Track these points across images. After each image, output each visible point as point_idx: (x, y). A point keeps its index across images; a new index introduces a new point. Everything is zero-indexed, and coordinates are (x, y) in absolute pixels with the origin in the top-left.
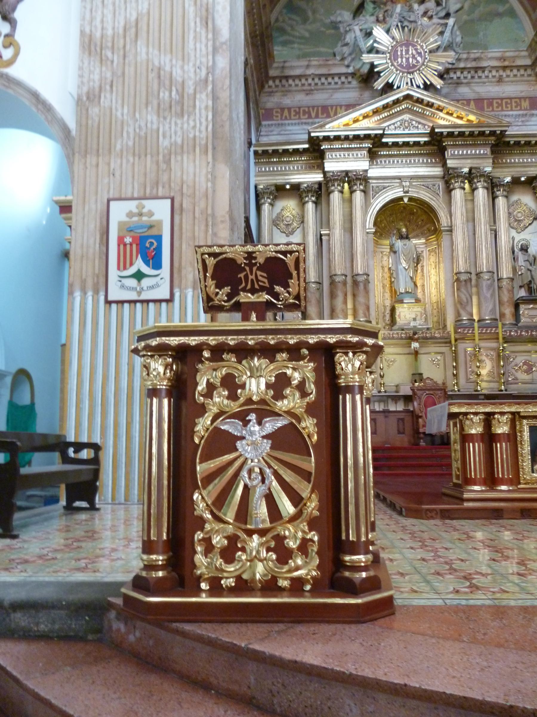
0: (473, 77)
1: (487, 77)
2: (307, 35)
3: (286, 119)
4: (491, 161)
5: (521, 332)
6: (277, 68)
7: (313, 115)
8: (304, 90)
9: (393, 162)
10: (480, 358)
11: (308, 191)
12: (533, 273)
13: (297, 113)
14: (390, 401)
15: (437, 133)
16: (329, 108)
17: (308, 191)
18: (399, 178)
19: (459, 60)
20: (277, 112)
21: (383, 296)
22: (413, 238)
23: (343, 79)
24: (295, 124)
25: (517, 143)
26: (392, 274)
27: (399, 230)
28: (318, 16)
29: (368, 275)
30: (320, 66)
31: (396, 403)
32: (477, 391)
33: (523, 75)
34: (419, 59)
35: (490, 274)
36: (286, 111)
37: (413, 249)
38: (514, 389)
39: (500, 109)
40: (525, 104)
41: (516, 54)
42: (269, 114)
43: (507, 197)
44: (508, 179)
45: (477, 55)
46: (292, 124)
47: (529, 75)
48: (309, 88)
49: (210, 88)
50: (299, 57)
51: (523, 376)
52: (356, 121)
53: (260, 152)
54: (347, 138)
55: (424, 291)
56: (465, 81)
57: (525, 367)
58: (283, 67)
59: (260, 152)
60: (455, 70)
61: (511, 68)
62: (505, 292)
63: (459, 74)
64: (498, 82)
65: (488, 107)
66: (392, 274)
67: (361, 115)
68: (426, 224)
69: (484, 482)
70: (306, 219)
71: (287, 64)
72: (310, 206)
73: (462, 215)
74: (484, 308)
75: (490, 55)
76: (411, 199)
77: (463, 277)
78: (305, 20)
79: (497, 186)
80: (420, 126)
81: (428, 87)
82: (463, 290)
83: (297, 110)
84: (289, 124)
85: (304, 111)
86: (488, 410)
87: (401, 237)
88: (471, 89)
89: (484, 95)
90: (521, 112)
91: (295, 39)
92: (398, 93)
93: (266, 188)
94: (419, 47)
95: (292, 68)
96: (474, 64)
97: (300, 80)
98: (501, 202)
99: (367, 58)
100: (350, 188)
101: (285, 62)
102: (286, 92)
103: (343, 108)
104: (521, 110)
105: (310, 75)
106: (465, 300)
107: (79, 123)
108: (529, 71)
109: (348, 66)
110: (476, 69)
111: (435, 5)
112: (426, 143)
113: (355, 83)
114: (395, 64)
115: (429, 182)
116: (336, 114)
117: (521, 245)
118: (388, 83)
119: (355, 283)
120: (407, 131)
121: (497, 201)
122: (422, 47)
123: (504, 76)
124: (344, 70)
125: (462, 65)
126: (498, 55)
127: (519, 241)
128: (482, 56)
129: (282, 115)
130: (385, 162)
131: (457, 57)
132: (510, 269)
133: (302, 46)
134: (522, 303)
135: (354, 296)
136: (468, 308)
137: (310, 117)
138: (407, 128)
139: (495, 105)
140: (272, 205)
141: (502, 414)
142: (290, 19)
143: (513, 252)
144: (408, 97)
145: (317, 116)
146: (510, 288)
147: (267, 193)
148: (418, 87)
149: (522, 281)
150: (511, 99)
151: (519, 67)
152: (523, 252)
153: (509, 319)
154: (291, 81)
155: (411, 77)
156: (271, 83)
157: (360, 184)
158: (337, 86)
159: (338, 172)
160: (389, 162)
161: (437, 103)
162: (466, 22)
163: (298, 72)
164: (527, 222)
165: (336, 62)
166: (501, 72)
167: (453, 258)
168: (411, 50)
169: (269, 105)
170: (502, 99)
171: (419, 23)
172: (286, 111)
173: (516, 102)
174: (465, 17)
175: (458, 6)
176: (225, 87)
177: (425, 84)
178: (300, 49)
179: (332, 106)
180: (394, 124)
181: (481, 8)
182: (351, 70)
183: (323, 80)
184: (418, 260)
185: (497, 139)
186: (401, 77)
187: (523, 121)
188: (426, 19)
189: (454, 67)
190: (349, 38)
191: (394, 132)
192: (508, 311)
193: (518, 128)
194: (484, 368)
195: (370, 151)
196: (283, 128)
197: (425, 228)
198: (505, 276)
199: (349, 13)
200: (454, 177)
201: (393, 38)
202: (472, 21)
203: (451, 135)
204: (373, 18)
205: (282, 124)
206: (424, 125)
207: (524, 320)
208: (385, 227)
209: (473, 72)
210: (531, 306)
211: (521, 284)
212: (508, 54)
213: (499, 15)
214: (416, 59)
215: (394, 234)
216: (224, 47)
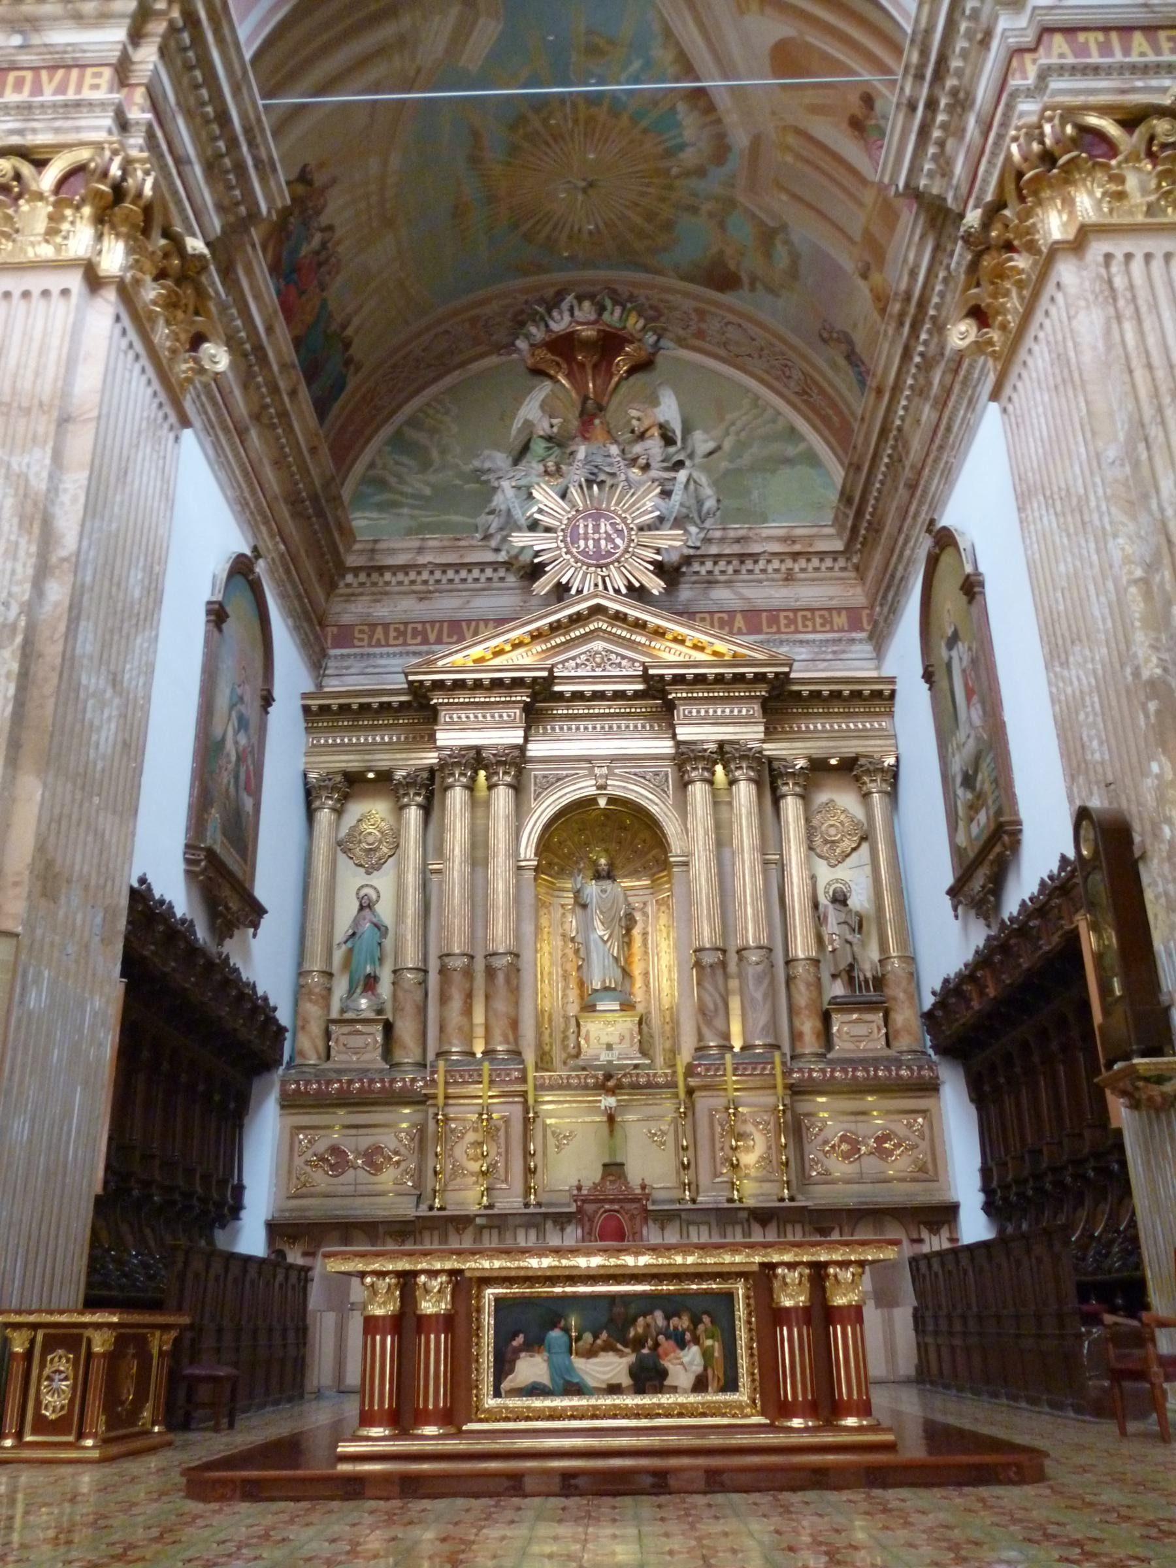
0: (736, 572)
1: (763, 571)
2: (428, 491)
3: (379, 645)
4: (762, 728)
6: (362, 551)
7: (432, 637)
8: (414, 592)
9: (578, 728)
10: (741, 1128)
11: (408, 785)
12: (855, 948)
13: (401, 634)
14: (549, 1225)
15: (653, 676)
16: (464, 624)
17: (408, 785)
18: (588, 759)
19: (707, 541)
20: (361, 632)
21: (564, 996)
22: (625, 876)
23: (489, 572)
24: (395, 655)
25: (815, 695)
26: (580, 950)
27: (595, 863)
28: (449, 457)
29: (517, 956)
30: (443, 549)
31: (562, 1230)
32: (731, 1200)
33: (817, 569)
34: (618, 541)
35: (763, 952)
36: (379, 629)
37: (621, 898)
38: (820, 1196)
39: (792, 628)
40: (841, 620)
41: (814, 531)
42: (345, 637)
43: (802, 797)
44: (801, 763)
45: (741, 533)
46: (388, 655)
47: (843, 569)
48: (424, 588)
49: (19, 639)
50: (409, 532)
51: (839, 1168)
52: (498, 653)
53: (314, 709)
54: (478, 685)
55: (647, 985)
56: (722, 578)
57: (844, 1147)
58: (373, 551)
59: (314, 709)
60: (702, 558)
61: (808, 556)
62: (802, 987)
63: (709, 565)
64: (786, 579)
65: (770, 626)
66: (580, 950)
67: (506, 641)
68: (651, 849)
69: (812, 1409)
70: (402, 842)
71: (381, 546)
72: (413, 815)
73: (706, 833)
74: (750, 1021)
75: (765, 533)
76: (612, 800)
77: (709, 959)
78: (426, 465)
79: (781, 775)
80: (624, 662)
81: (638, 593)
82: (707, 985)
83: (402, 628)
84: (381, 655)
85: (414, 629)
86: (403, 1265)
87: (598, 876)
88: (736, 593)
89: (761, 604)
90: (829, 636)
91: (404, 500)
92: (578, 603)
93: (329, 776)
94: (618, 520)
95: (392, 552)
96: (737, 549)
97: (407, 574)
98: (791, 807)
99: (520, 539)
100: (488, 778)
101: (376, 541)
102: (380, 595)
103: (491, 624)
104: (832, 631)
105: (424, 566)
106: (711, 1006)
108: (841, 562)
109: (497, 550)
110: (742, 558)
111: (662, 443)
112: (637, 695)
113: (512, 579)
114: (574, 550)
115: (650, 769)
116: (476, 633)
117: (835, 892)
118: (559, 584)
120: (598, 672)
121: (782, 803)
122: (624, 520)
123: (797, 569)
124: (490, 557)
125: (714, 550)
126: (781, 532)
127: (829, 884)
128: (751, 534)
129: (371, 637)
130: (561, 729)
131: (702, 535)
132: (812, 941)
133: (417, 512)
134: (838, 1011)
136: (719, 1023)
137: (425, 641)
138: (599, 666)
139: (783, 622)
140: (339, 812)
141: (433, 1274)
142: (397, 463)
143: (816, 906)
144: (598, 610)
145: (439, 641)
146: (811, 979)
147: (326, 787)
148: (617, 591)
149: (836, 965)
150: (812, 610)
151: (822, 555)
152: (838, 906)
153: (810, 1044)
154: (388, 576)
155: (605, 572)
156: (349, 578)
157: (505, 773)
158: (478, 586)
159: (462, 748)
160: (570, 729)
161: (653, 621)
162: (727, 473)
163: (401, 559)
164: (847, 844)
165: (474, 543)
166: (789, 563)
167: (690, 920)
168: (605, 526)
169: (346, 619)
170: (795, 611)
171: (623, 477)
172: (379, 629)
173: (822, 616)
174: (724, 465)
175: (711, 445)
176: (56, 636)
177: (630, 587)
178: (412, 517)
179: (469, 622)
180: (573, 658)
181: (754, 450)
182: (502, 557)
183: (438, 575)
184: (629, 922)
185: (773, 688)
186: (585, 574)
187: (834, 652)
188: (635, 470)
189: (699, 552)
190: (498, 501)
191: (573, 674)
192: (808, 1026)
193: (825, 664)
194: (748, 1150)
195: (528, 709)
196: (372, 662)
197: (650, 856)
198: (801, 955)
199: (504, 455)
200: (689, 759)
201: (573, 505)
202: (738, 471)
203: (679, 680)
204: (541, 468)
205: (369, 655)
206: (633, 661)
207: (842, 1047)
208: (572, 854)
209: (735, 562)
210: (855, 1016)
211: (833, 971)
212: (799, 532)
213: (788, 461)
214: (613, 541)
215: (580, 871)
216: (66, 565)
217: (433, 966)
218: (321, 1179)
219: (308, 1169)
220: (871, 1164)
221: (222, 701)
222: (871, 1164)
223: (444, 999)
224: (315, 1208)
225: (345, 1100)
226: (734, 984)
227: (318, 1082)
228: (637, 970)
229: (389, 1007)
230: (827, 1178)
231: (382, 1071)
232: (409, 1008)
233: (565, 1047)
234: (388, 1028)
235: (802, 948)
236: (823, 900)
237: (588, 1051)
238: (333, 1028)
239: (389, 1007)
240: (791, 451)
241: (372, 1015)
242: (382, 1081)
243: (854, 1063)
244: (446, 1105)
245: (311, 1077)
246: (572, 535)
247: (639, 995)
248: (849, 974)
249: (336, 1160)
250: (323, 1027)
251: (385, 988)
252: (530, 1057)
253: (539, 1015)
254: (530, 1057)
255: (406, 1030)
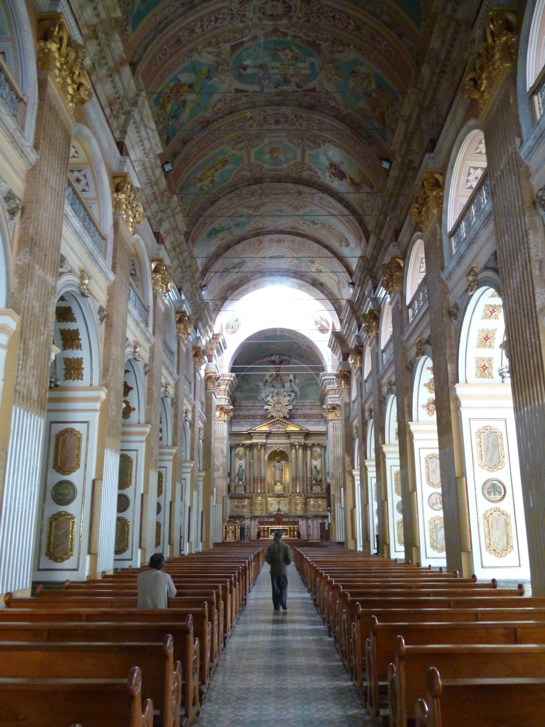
13: (244, 417)
25: (313, 434)
26: (274, 474)
51: (313, 509)
66: (274, 474)
77: (294, 478)
78: (248, 383)
99: (266, 407)
119: (261, 480)
124: (260, 405)
135: (261, 483)
153: (309, 491)
184: (282, 470)
192: (309, 488)
207: (314, 491)
213: (312, 384)
217: (252, 479)
218: (235, 509)
220: (317, 509)
222: (317, 509)
224: (234, 514)
225: (239, 498)
228: (283, 477)
230: (311, 511)
234: (245, 487)
235: (309, 476)
236: (313, 467)
237: (275, 490)
240: (314, 382)
243: (315, 494)
246: (274, 407)
248: (316, 480)
249: (237, 507)
251: (244, 480)
252: (267, 492)
253: (268, 484)
254: (267, 492)
255: (247, 487)
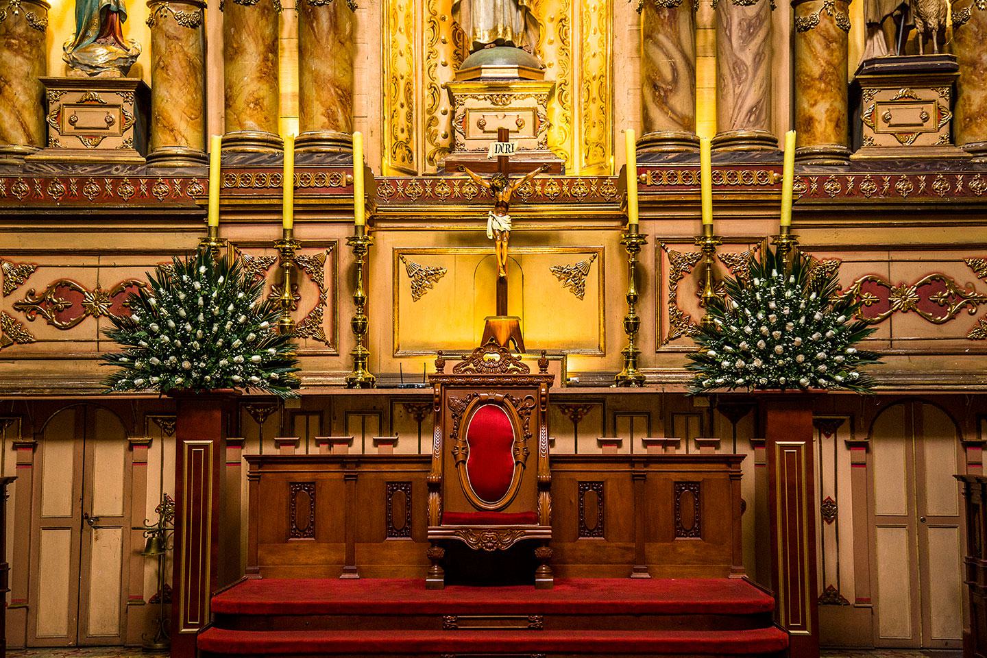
5: (894, 180)
74: (730, 100)
107: (776, 254)
134: (869, 82)
136: (679, 102)
219: (21, 316)
221: (588, 396)
223: (231, 53)
226: (706, 38)
227: (30, 181)
229: (145, 61)
231: (134, 165)
232: (177, 65)
233: (432, 137)
238: (51, 93)
239: (145, 61)
241: (115, 74)
242: (135, 181)
244: (221, 223)
245: (19, 173)
247: (550, 53)
250: (35, 91)
